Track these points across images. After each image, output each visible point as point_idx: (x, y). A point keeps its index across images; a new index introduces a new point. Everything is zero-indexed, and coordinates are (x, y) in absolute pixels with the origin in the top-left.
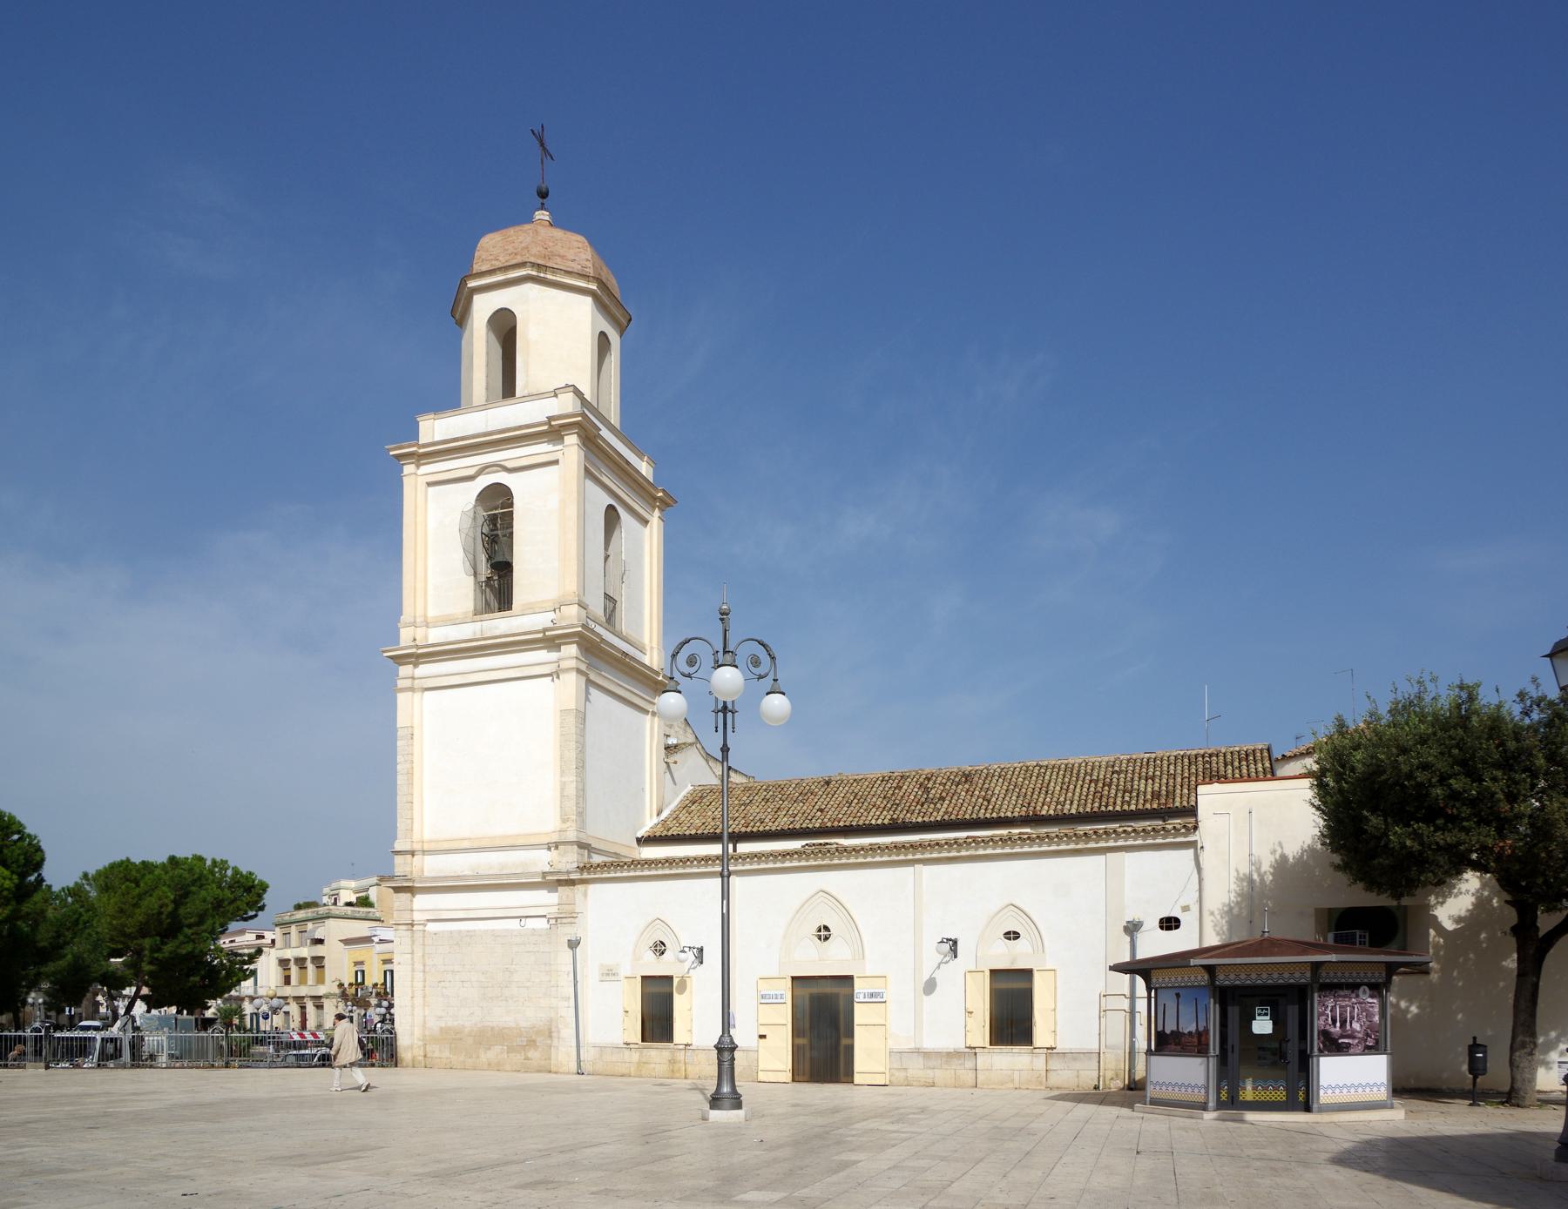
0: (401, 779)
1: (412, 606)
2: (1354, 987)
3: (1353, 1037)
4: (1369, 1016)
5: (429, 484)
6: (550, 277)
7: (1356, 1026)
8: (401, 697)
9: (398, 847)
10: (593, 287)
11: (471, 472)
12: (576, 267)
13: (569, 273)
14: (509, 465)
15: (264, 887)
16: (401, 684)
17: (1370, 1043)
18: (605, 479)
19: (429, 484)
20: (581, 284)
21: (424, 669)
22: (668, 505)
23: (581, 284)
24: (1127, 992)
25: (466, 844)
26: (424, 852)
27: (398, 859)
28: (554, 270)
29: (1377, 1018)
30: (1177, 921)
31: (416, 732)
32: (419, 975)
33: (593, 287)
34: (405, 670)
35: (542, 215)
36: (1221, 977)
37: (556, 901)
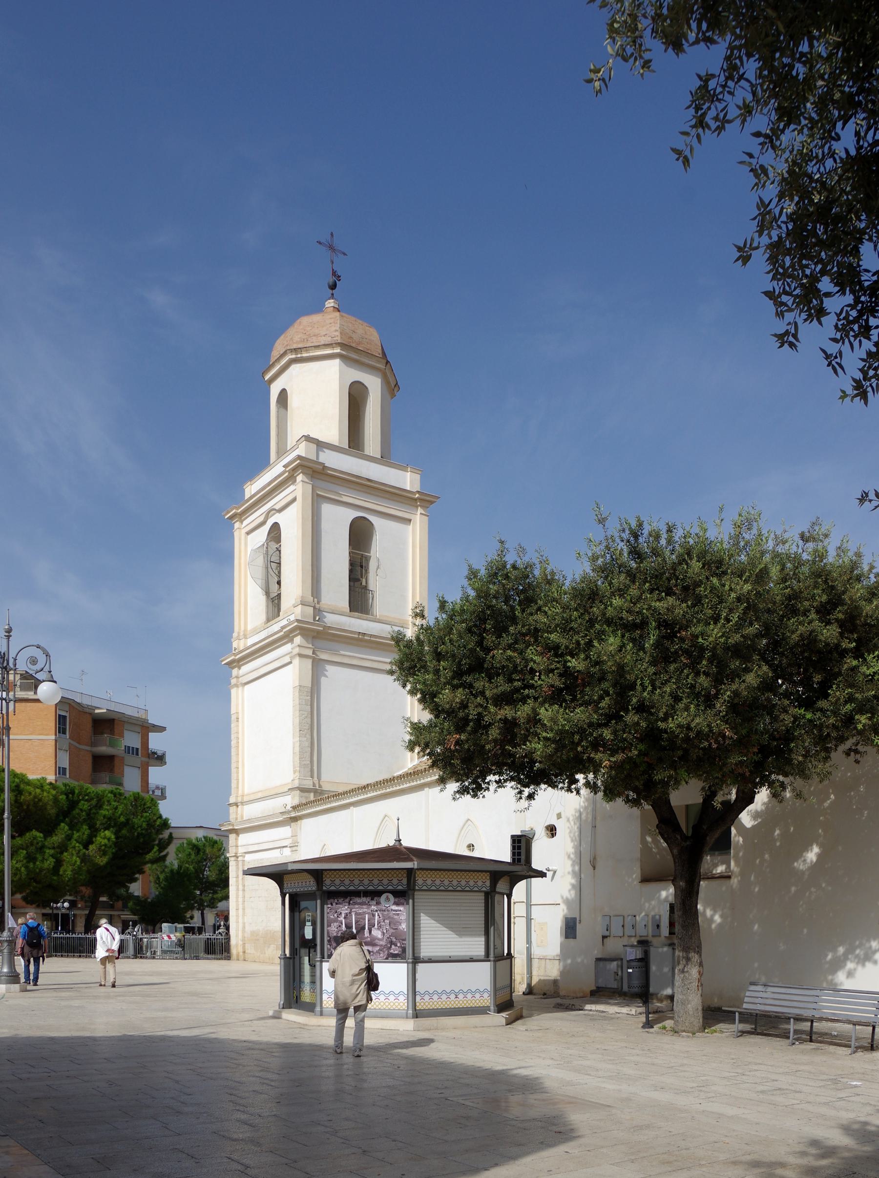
0: (233, 752)
1: (239, 626)
2: (374, 894)
3: (374, 945)
4: (393, 923)
5: (248, 533)
6: (305, 355)
7: (377, 933)
8: (233, 691)
9: (232, 800)
10: (337, 350)
11: (261, 519)
12: (327, 340)
13: (317, 347)
14: (277, 507)
15: (512, 836)
16: (233, 681)
17: (395, 950)
18: (345, 499)
19: (248, 533)
20: (328, 351)
21: (245, 669)
22: (432, 502)
23: (328, 351)
24: (535, 910)
25: (260, 795)
26: (242, 803)
27: (232, 809)
28: (306, 349)
29: (403, 926)
30: (553, 835)
31: (240, 717)
32: (241, 893)
33: (337, 350)
34: (235, 672)
35: (330, 303)
36: (327, 882)
37: (290, 835)
